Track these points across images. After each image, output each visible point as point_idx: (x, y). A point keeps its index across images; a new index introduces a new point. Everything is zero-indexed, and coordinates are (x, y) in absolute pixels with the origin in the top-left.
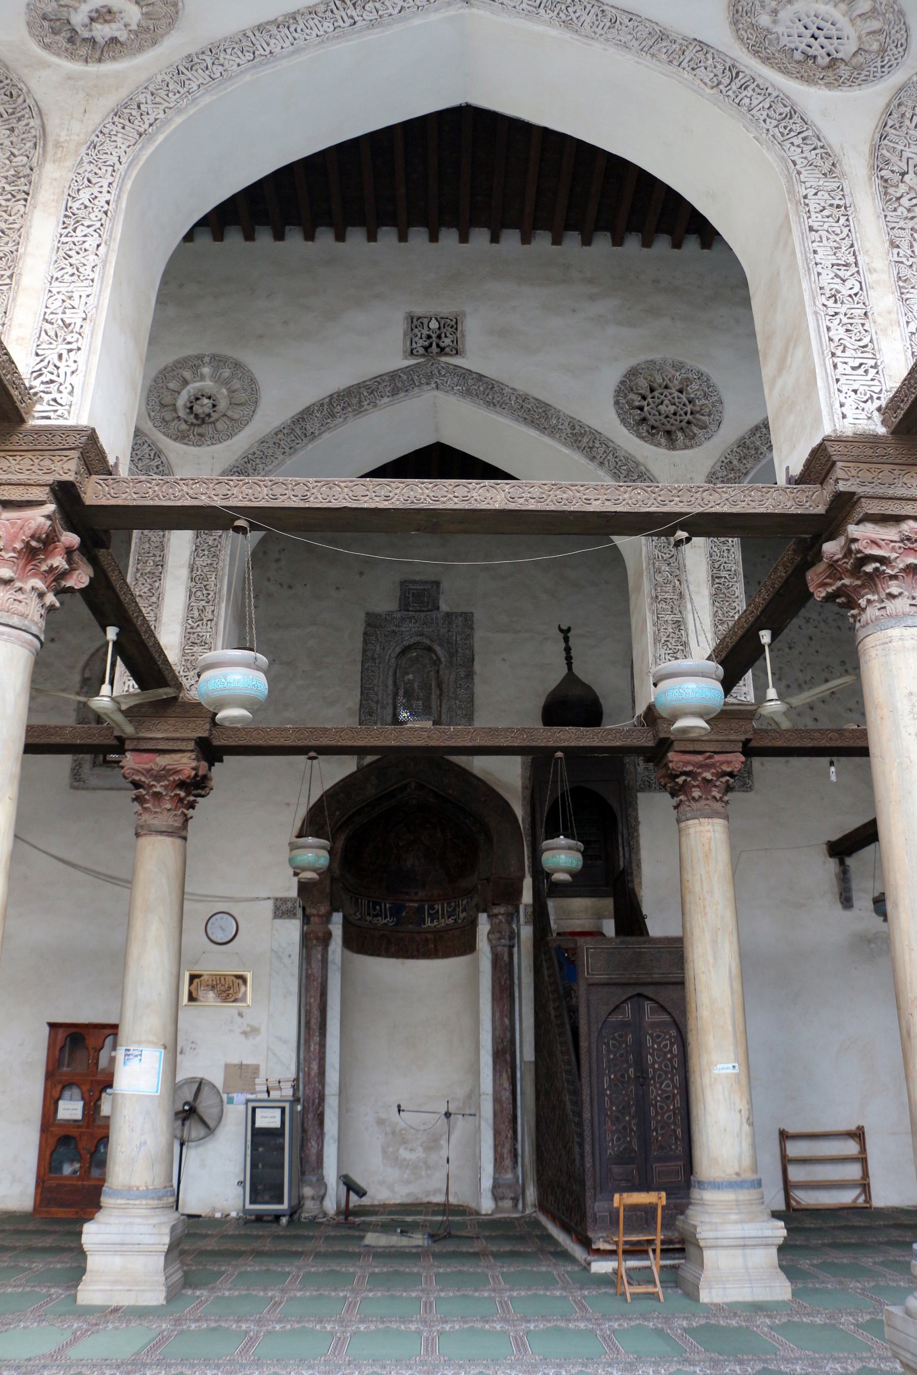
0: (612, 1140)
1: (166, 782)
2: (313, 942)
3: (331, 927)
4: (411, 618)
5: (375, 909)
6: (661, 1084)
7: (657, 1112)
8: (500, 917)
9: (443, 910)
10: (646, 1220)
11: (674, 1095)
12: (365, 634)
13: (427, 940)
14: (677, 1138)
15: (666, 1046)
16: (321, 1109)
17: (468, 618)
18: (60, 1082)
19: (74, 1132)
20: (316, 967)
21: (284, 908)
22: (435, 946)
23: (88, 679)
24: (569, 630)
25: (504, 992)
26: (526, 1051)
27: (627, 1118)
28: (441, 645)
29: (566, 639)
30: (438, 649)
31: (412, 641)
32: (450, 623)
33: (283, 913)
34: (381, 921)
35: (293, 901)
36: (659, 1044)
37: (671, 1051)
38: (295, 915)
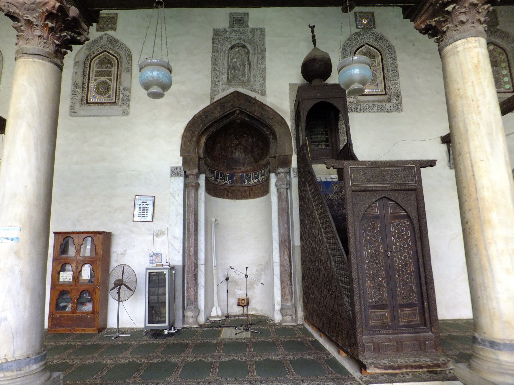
0: (371, 293)
1: (37, 14)
2: (190, 187)
3: (199, 181)
4: (235, 31)
5: (221, 176)
6: (401, 255)
7: (400, 275)
8: (281, 174)
9: (252, 176)
10: (398, 348)
11: (410, 263)
12: (213, 39)
13: (245, 191)
14: (413, 291)
15: (403, 231)
16: (195, 272)
17: (262, 31)
18: (60, 263)
19: (68, 288)
20: (192, 201)
21: (175, 171)
22: (250, 193)
23: (78, 62)
24: (314, 27)
25: (284, 212)
26: (297, 241)
27: (380, 279)
28: (250, 44)
29: (313, 31)
30: (248, 46)
31: (236, 42)
32: (254, 33)
33: (175, 174)
34: (224, 182)
35: (180, 168)
36: (398, 230)
37: (406, 235)
38: (181, 175)
